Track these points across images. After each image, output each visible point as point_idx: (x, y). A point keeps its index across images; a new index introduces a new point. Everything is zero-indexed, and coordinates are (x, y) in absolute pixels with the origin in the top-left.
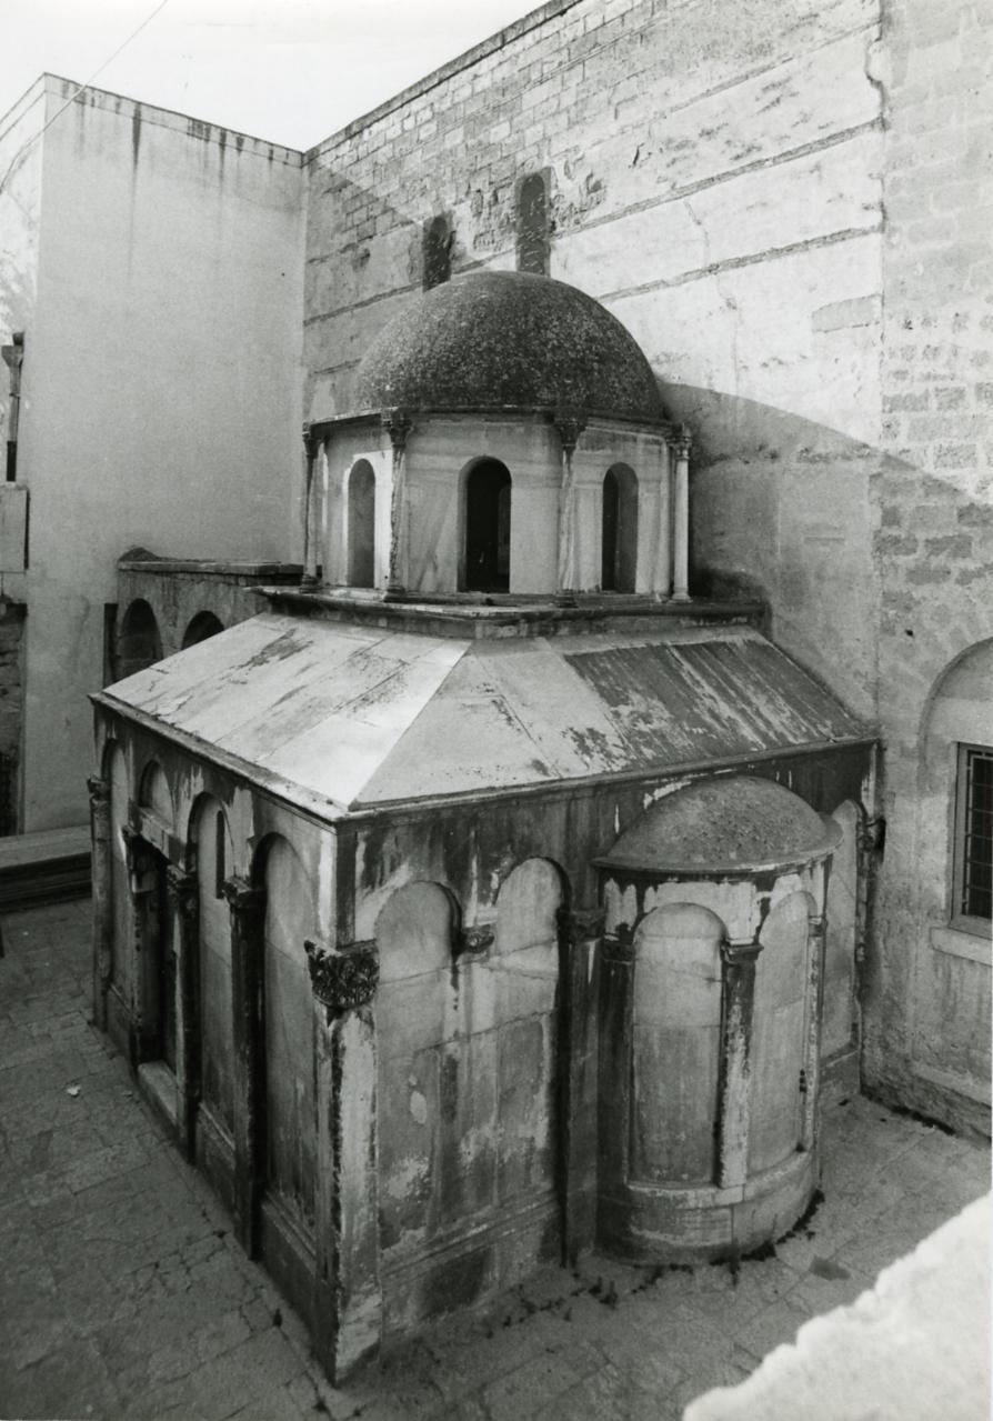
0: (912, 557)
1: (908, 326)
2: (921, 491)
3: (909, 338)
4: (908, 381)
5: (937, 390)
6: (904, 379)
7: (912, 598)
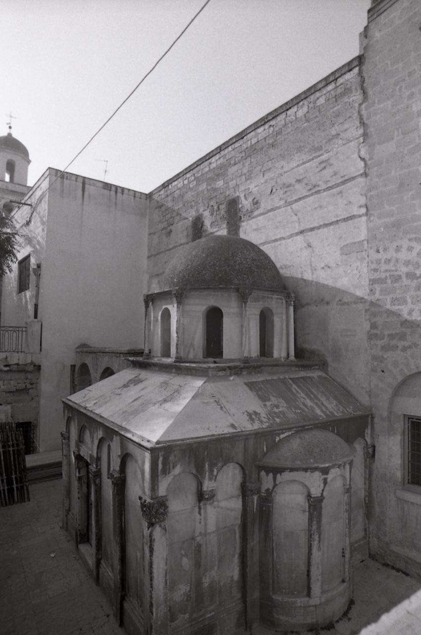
0: (383, 341)
1: (378, 251)
2: (385, 315)
3: (379, 256)
4: (378, 273)
5: (390, 275)
6: (377, 272)
7: (383, 358)
